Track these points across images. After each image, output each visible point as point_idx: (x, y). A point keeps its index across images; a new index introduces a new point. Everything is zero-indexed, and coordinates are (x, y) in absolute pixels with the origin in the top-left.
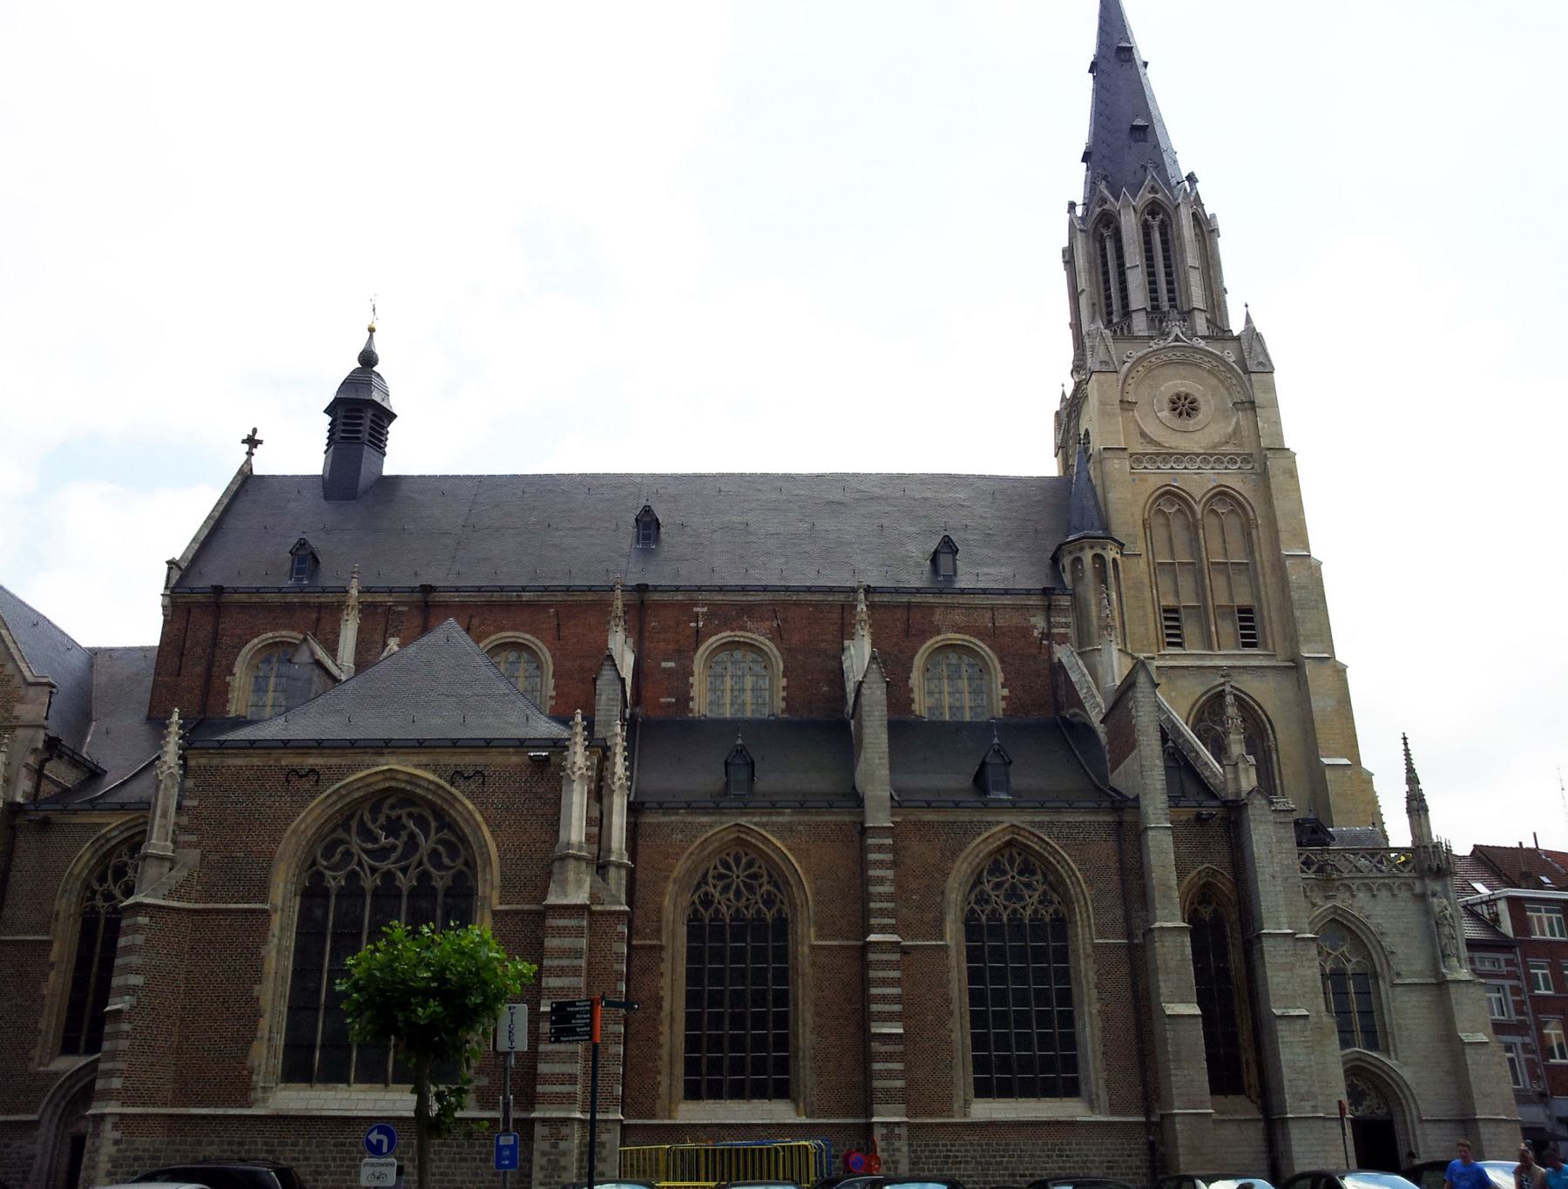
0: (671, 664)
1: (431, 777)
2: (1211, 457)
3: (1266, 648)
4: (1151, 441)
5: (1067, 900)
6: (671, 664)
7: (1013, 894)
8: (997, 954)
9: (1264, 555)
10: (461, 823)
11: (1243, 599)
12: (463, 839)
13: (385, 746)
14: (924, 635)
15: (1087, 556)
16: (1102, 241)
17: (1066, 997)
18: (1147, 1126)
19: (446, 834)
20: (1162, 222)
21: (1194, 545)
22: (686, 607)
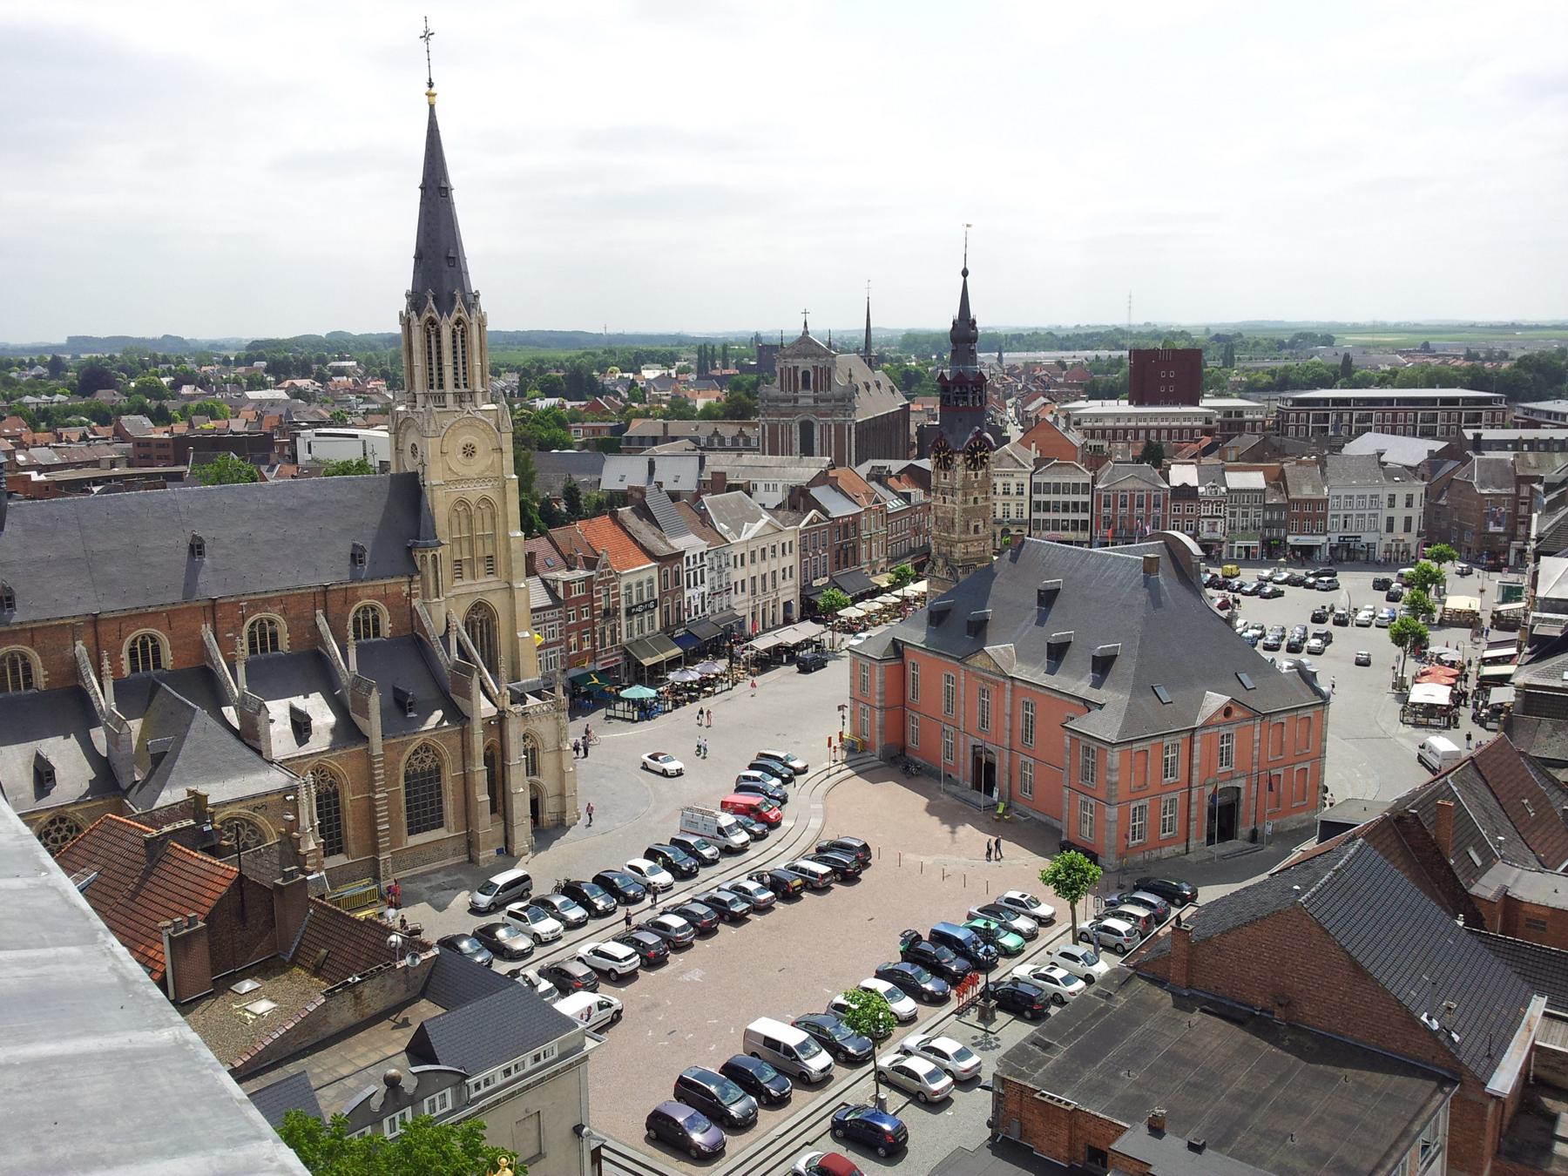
2: (481, 479)
5: (441, 760)
7: (422, 761)
9: (500, 531)
10: (716, 1165)
11: (489, 552)
12: (259, 828)
13: (227, 804)
14: (354, 602)
15: (429, 555)
19: (251, 827)
20: (458, 322)
21: (470, 529)
22: (235, 604)
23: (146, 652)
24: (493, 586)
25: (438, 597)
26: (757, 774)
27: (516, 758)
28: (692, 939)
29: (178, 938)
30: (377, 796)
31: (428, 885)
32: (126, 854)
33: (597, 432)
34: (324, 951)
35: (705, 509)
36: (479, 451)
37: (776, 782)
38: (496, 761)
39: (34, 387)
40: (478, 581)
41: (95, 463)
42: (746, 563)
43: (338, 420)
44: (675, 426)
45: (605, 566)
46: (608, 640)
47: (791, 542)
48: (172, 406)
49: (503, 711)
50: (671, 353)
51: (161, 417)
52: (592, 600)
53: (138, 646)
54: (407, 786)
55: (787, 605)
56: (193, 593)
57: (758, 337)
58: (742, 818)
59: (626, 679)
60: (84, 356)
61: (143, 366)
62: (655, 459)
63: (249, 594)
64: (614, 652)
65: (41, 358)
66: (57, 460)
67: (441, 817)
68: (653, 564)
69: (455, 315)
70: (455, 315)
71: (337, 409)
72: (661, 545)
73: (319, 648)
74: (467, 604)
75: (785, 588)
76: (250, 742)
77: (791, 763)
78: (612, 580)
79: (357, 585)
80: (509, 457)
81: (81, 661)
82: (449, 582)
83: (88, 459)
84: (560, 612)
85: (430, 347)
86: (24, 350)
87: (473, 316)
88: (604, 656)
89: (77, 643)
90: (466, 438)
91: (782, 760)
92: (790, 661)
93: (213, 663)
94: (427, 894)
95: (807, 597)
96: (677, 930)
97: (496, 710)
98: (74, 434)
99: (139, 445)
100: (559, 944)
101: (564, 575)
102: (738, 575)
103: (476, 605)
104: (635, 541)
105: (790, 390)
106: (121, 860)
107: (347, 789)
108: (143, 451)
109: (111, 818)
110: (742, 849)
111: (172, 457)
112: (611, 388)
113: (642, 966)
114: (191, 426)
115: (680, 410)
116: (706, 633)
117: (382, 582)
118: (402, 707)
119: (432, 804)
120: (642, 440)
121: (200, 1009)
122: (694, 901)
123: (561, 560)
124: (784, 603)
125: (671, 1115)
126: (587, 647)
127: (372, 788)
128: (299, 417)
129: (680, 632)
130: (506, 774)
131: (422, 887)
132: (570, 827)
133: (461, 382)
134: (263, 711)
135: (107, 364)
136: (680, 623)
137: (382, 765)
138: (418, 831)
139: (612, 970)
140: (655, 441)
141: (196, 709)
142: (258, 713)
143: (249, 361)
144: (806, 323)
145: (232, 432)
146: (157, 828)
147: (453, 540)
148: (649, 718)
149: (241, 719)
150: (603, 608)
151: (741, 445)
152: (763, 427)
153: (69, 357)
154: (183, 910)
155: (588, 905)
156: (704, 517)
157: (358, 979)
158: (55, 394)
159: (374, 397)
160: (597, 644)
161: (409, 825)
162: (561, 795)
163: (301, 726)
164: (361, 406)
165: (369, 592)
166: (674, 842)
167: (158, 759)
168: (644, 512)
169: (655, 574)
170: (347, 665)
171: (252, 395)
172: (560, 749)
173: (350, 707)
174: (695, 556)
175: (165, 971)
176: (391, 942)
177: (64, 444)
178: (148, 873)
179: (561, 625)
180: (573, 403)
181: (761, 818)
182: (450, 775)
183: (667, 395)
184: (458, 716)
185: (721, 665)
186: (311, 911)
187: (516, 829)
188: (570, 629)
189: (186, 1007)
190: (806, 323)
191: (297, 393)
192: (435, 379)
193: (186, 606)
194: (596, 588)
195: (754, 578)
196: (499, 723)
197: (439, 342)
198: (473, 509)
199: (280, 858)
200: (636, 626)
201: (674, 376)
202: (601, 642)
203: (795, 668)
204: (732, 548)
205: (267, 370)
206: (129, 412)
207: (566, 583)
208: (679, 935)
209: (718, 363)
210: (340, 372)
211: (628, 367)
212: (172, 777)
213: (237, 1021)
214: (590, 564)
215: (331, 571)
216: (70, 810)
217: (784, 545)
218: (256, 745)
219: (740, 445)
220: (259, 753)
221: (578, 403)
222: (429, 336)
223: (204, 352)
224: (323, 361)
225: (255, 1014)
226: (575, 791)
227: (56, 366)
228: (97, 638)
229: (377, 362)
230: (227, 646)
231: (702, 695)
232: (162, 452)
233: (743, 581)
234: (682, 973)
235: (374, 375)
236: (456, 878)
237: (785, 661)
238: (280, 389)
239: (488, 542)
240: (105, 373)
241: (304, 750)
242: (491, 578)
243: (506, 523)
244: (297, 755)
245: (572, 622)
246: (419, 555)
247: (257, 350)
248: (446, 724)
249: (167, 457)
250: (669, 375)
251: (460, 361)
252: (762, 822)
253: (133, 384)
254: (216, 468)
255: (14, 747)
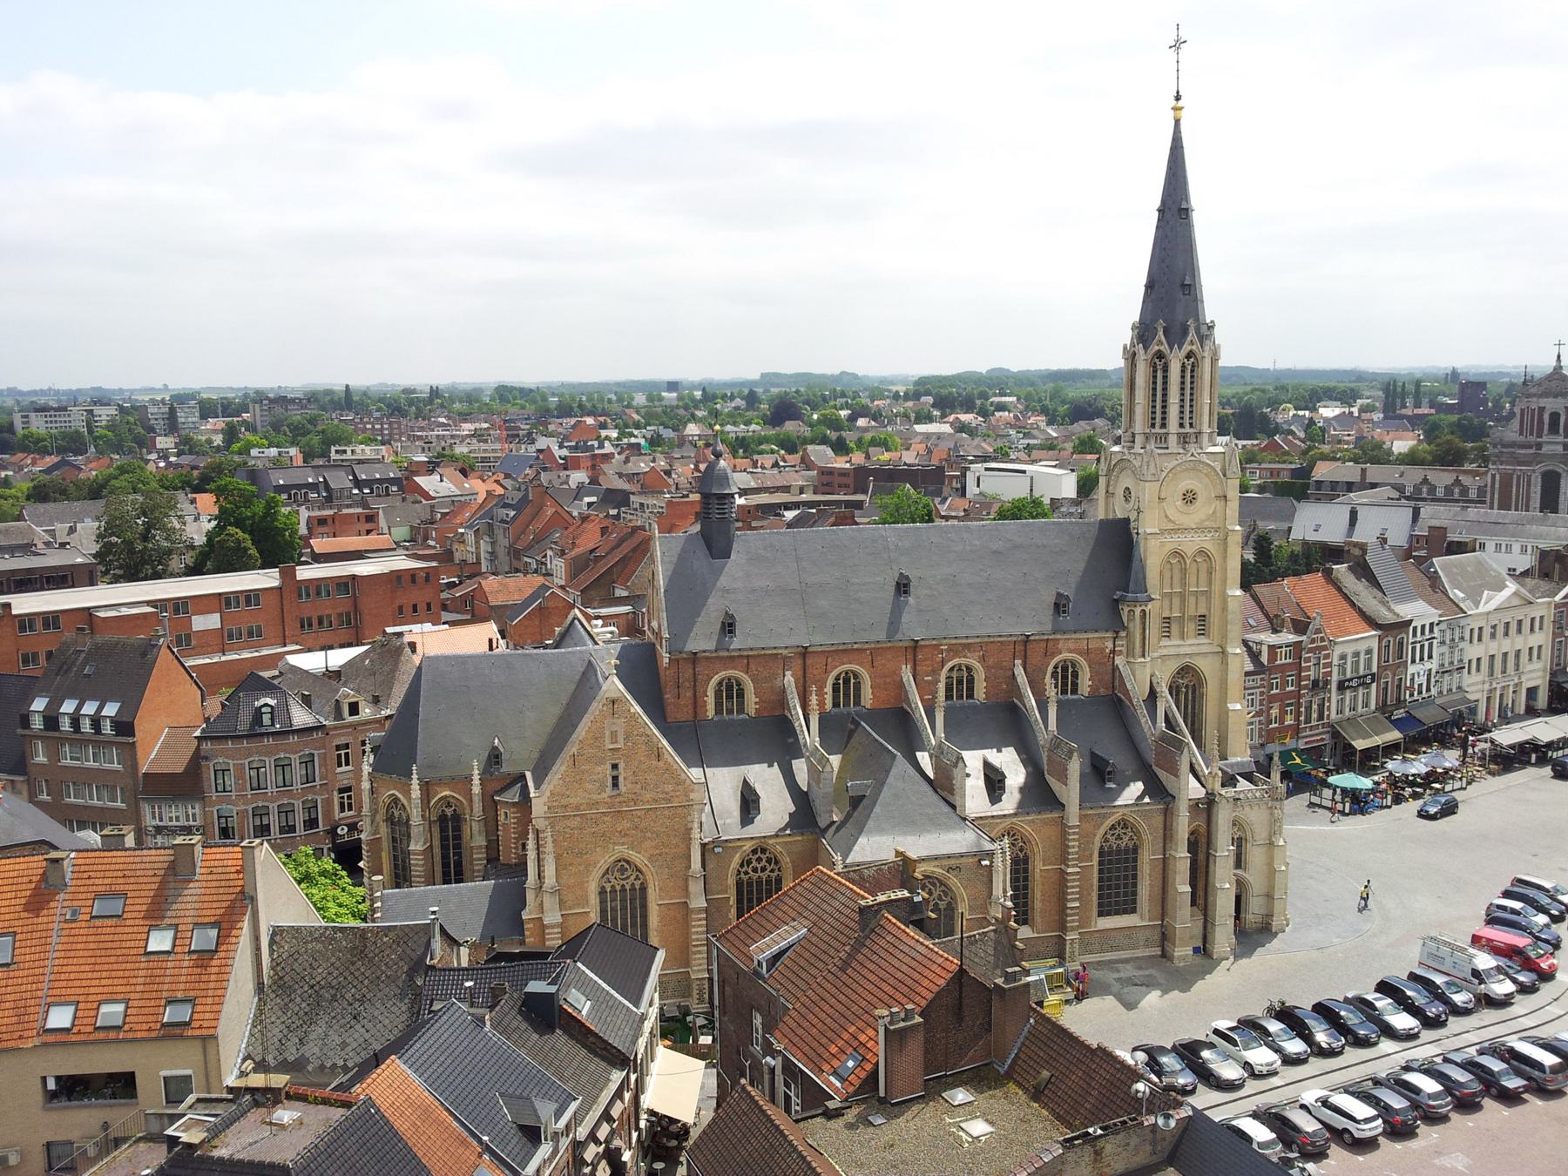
0: (930, 678)
1: (941, 871)
2: (1200, 529)
3: (1209, 638)
4: (1170, 521)
6: (930, 678)
8: (1110, 862)
9: (1216, 588)
11: (1202, 611)
12: (950, 889)
14: (1053, 655)
15: (1138, 611)
16: (1155, 366)
17: (1135, 877)
18: (1162, 925)
20: (1188, 357)
21: (1183, 584)
23: (847, 687)
24: (1204, 649)
25: (1144, 656)
26: (1517, 905)
27: (1224, 849)
28: (1449, 1111)
29: (895, 1031)
30: (1070, 870)
31: (1117, 975)
32: (837, 915)
33: (1275, 474)
34: (1045, 1074)
35: (1436, 572)
36: (1201, 498)
37: (1542, 919)
38: (1201, 847)
39: (734, 417)
40: (1189, 642)
41: (786, 489)
42: (1484, 639)
43: (1001, 455)
44: (1375, 472)
45: (1318, 631)
46: (1315, 716)
47: (1542, 617)
48: (850, 437)
49: (1213, 794)
50: (1352, 390)
51: (840, 448)
52: (1300, 669)
53: (841, 681)
54: (1101, 863)
55: (1532, 692)
56: (896, 631)
57: (1454, 375)
58: (1502, 962)
59: (1332, 761)
60: (775, 390)
61: (825, 399)
62: (1358, 508)
63: (950, 638)
64: (1321, 730)
65: (740, 392)
66: (753, 484)
67: (1134, 901)
68: (1374, 633)
69: (1187, 348)
70: (1187, 348)
71: (999, 443)
72: (1383, 611)
73: (1015, 700)
74: (1173, 666)
75: (1530, 671)
76: (944, 794)
77: (1560, 897)
78: (1325, 648)
79: (1059, 636)
80: (1233, 507)
81: (788, 692)
82: (1156, 640)
83: (778, 484)
84: (1262, 679)
85: (1155, 383)
86: (726, 385)
87: (1207, 348)
88: (1308, 733)
89: (787, 673)
90: (1187, 483)
91: (1548, 891)
92: (1542, 761)
93: (910, 706)
94: (1116, 987)
95: (1559, 684)
96: (1430, 1096)
97: (1204, 791)
98: (768, 460)
99: (823, 473)
100: (1275, 1081)
101: (1273, 639)
102: (1473, 651)
103: (1182, 669)
104: (1353, 604)
105: (1532, 434)
106: (831, 921)
107: (1037, 857)
108: (826, 479)
109: (822, 872)
110: (1504, 1003)
111: (852, 486)
112: (1285, 427)
113: (1385, 1133)
114: (868, 457)
115: (1371, 453)
116: (1429, 716)
117: (1085, 636)
118: (1100, 774)
119: (1126, 886)
120: (1334, 485)
121: (909, 1115)
122: (1446, 1060)
123: (1266, 621)
124: (1528, 689)
125: (1110, 1049)
126: (1289, 721)
127: (1064, 859)
128: (966, 451)
129: (1399, 714)
130: (1211, 866)
131: (1110, 977)
132: (1276, 934)
133: (1187, 421)
134: (960, 764)
135: (794, 398)
136: (1400, 703)
137: (1076, 837)
138: (1109, 914)
139: (1346, 1130)
140: (1350, 487)
141: (895, 756)
142: (956, 765)
143: (916, 396)
144: (1559, 356)
145: (905, 464)
146: (873, 894)
147: (1164, 595)
148: (1363, 812)
149: (936, 769)
150: (1312, 678)
151: (1456, 496)
152: (1493, 476)
153: (761, 390)
154: (904, 1001)
155: (1307, 1037)
156: (1434, 580)
157: (1099, 1132)
158: (751, 423)
159: (1035, 432)
160: (1302, 718)
161: (1100, 905)
162: (1269, 896)
163: (994, 782)
164: (1022, 441)
165: (1071, 645)
166: (1414, 977)
167: (856, 802)
168: (1363, 570)
169: (1375, 645)
170: (1047, 727)
171: (919, 428)
172: (1271, 844)
173: (1046, 767)
174: (1423, 627)
175: (877, 1064)
176: (1137, 1091)
177: (759, 470)
178: (859, 945)
179: (1262, 694)
180: (1245, 442)
181: (1529, 965)
182: (1147, 859)
183: (1350, 436)
184: (1157, 790)
185: (1451, 758)
186: (1032, 1021)
187: (1217, 929)
188: (1272, 699)
189: (896, 1109)
190: (1559, 356)
191: (961, 428)
192: (1158, 417)
193: (889, 645)
194: (1305, 655)
195: (1492, 657)
196: (1206, 807)
197: (1165, 377)
198: (1188, 562)
199: (995, 949)
200: (1347, 702)
201: (1356, 414)
202: (1306, 716)
203: (1547, 771)
204: (1468, 620)
205: (934, 406)
206: (812, 442)
207: (1272, 648)
208: (1431, 1103)
209: (1409, 402)
210: (1001, 407)
211: (1303, 404)
212: (870, 823)
213: (951, 1139)
214: (1300, 627)
215: (1034, 621)
216: (771, 842)
217: (1533, 619)
218: (950, 798)
219: (1456, 496)
220: (953, 807)
221: (1250, 442)
222: (1155, 371)
223: (877, 388)
224: (984, 396)
225: (972, 1137)
226: (1286, 893)
227: (752, 399)
228: (805, 669)
229: (1036, 398)
230: (926, 690)
231: (1428, 791)
232: (843, 480)
233: (1479, 660)
234: (1439, 1153)
235: (1034, 410)
236: (1147, 972)
237: (1533, 760)
238: (945, 422)
239: (1202, 599)
240: (792, 405)
241: (997, 810)
242: (1202, 640)
243: (1224, 581)
244: (989, 814)
245: (1274, 691)
246: (1126, 609)
247: (922, 387)
248: (1147, 800)
249: (847, 486)
250: (1351, 413)
251: (1188, 397)
252: (1530, 970)
253: (815, 417)
254: (895, 499)
255: (725, 770)
